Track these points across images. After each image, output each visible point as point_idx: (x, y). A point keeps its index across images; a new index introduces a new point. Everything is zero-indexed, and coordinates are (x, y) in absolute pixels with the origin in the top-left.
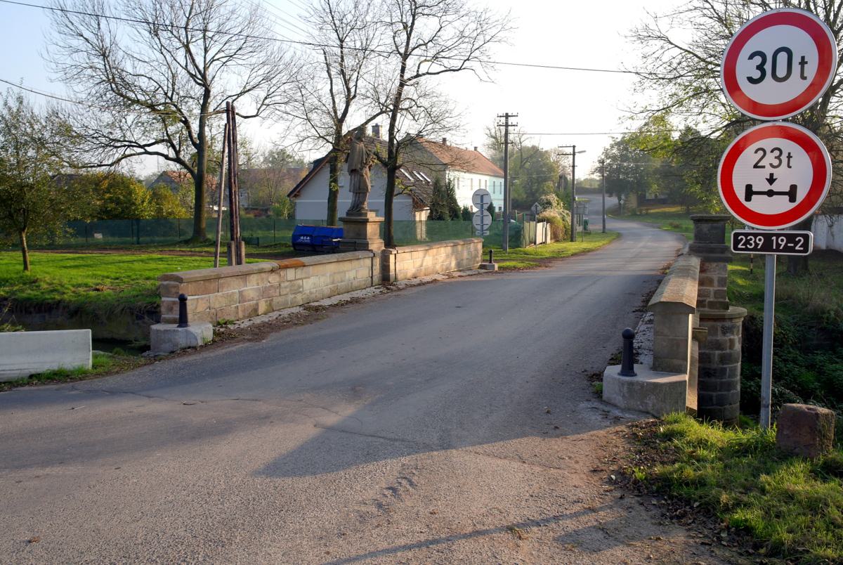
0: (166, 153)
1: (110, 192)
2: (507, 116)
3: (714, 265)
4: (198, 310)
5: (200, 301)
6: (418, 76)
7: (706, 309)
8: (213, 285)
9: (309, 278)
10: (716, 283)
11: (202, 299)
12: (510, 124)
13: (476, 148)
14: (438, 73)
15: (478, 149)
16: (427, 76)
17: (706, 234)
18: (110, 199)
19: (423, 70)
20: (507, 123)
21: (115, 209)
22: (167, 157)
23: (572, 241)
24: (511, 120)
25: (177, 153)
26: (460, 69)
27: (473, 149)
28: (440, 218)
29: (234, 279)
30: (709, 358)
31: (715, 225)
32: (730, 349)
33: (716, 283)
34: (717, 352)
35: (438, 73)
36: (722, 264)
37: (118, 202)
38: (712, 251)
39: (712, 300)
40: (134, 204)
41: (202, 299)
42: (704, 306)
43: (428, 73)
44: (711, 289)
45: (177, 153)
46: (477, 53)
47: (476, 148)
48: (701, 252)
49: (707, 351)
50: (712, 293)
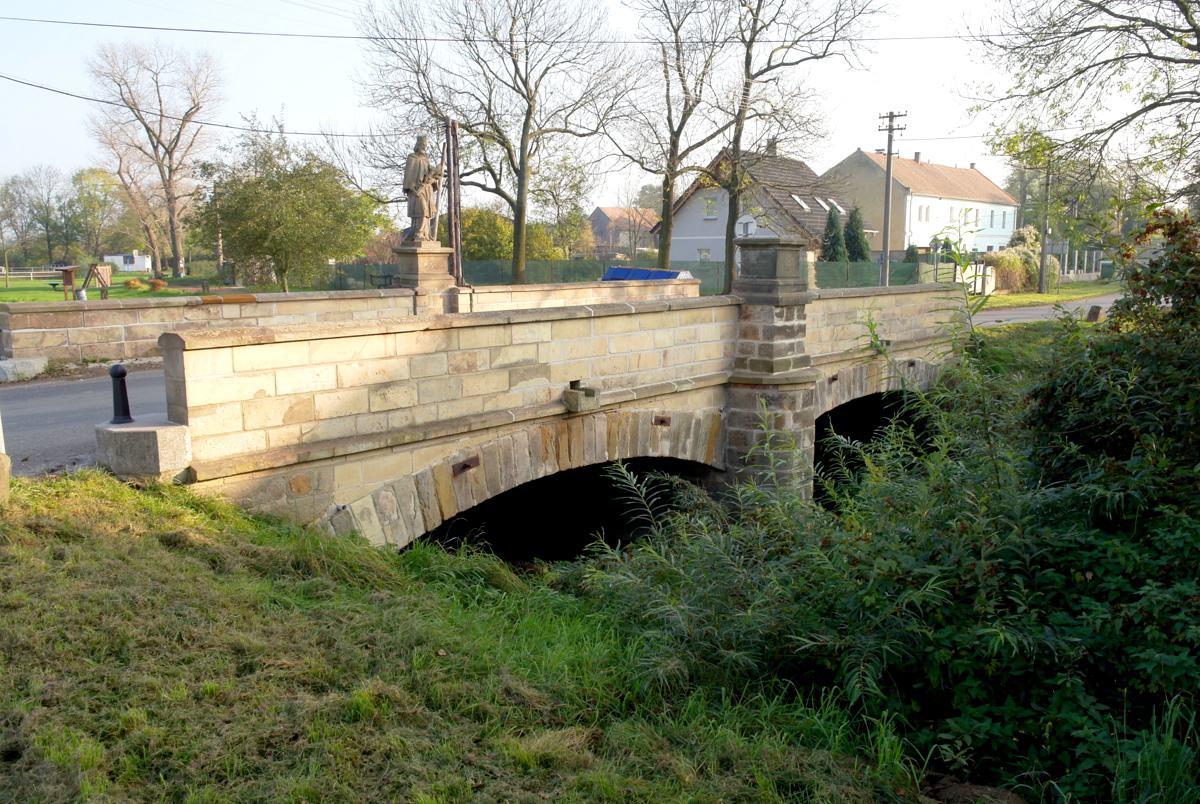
0: (483, 183)
1: (473, 232)
2: (891, 116)
3: (759, 308)
4: (45, 345)
5: (48, 335)
6: (770, 68)
7: (748, 371)
8: (72, 318)
9: (271, 316)
10: (761, 335)
11: (53, 333)
12: (895, 126)
13: (972, 165)
14: (797, 63)
15: (976, 167)
16: (782, 68)
17: (753, 265)
18: (474, 239)
19: (777, 59)
20: (891, 120)
21: (479, 251)
22: (484, 188)
23: (1040, 292)
24: (897, 122)
25: (497, 182)
26: (824, 56)
27: (968, 167)
28: (833, 259)
29: (114, 312)
30: (745, 438)
31: (764, 252)
32: (776, 428)
33: (761, 335)
34: (755, 431)
35: (797, 63)
36: (768, 308)
37: (481, 242)
38: (757, 289)
39: (756, 357)
40: (500, 245)
41: (53, 333)
42: (744, 367)
43: (783, 64)
44: (756, 342)
45: (497, 182)
46: (841, 34)
47: (972, 165)
48: (744, 290)
49: (743, 430)
50: (757, 349)
